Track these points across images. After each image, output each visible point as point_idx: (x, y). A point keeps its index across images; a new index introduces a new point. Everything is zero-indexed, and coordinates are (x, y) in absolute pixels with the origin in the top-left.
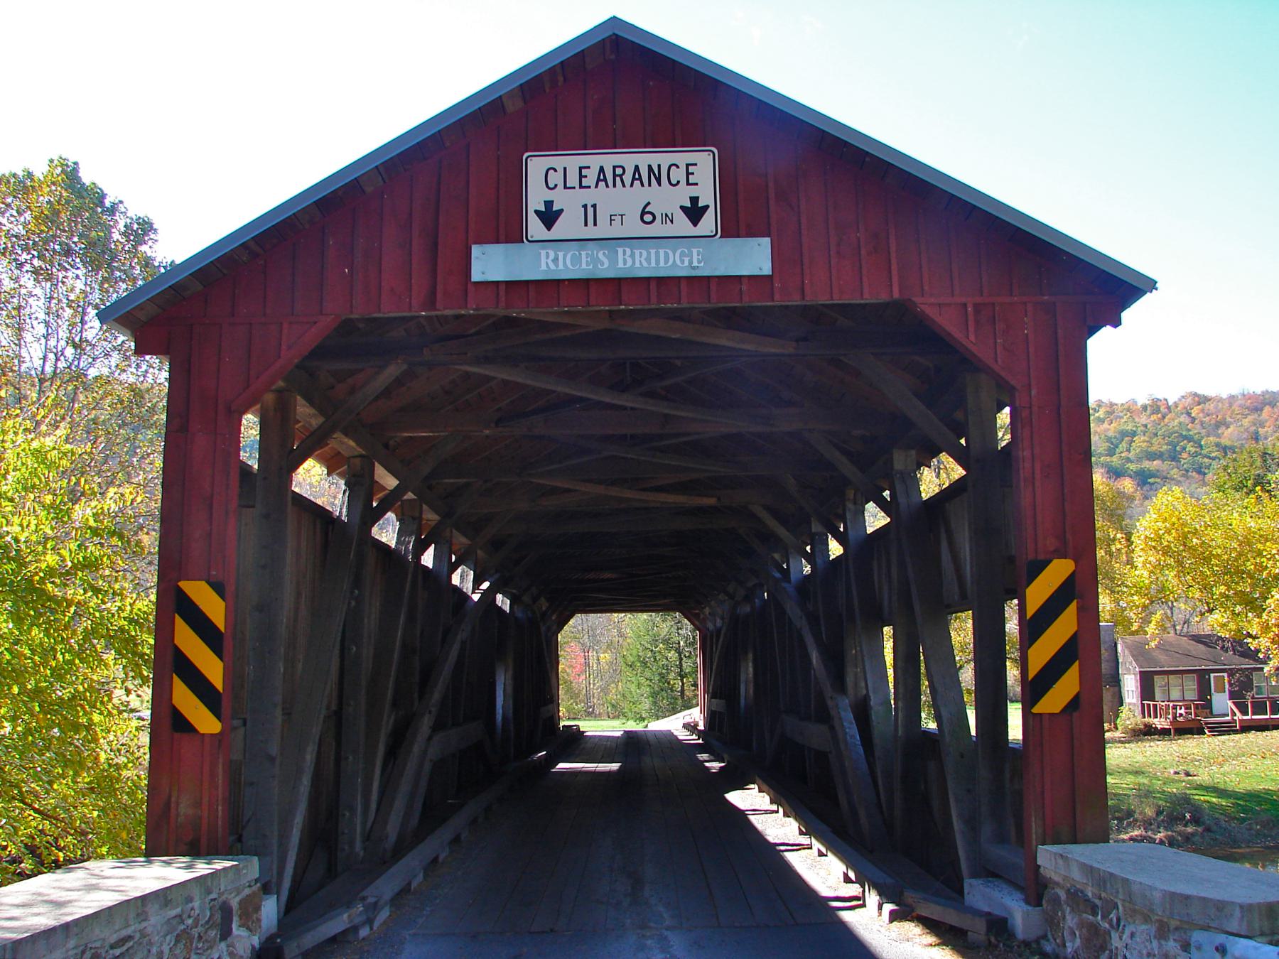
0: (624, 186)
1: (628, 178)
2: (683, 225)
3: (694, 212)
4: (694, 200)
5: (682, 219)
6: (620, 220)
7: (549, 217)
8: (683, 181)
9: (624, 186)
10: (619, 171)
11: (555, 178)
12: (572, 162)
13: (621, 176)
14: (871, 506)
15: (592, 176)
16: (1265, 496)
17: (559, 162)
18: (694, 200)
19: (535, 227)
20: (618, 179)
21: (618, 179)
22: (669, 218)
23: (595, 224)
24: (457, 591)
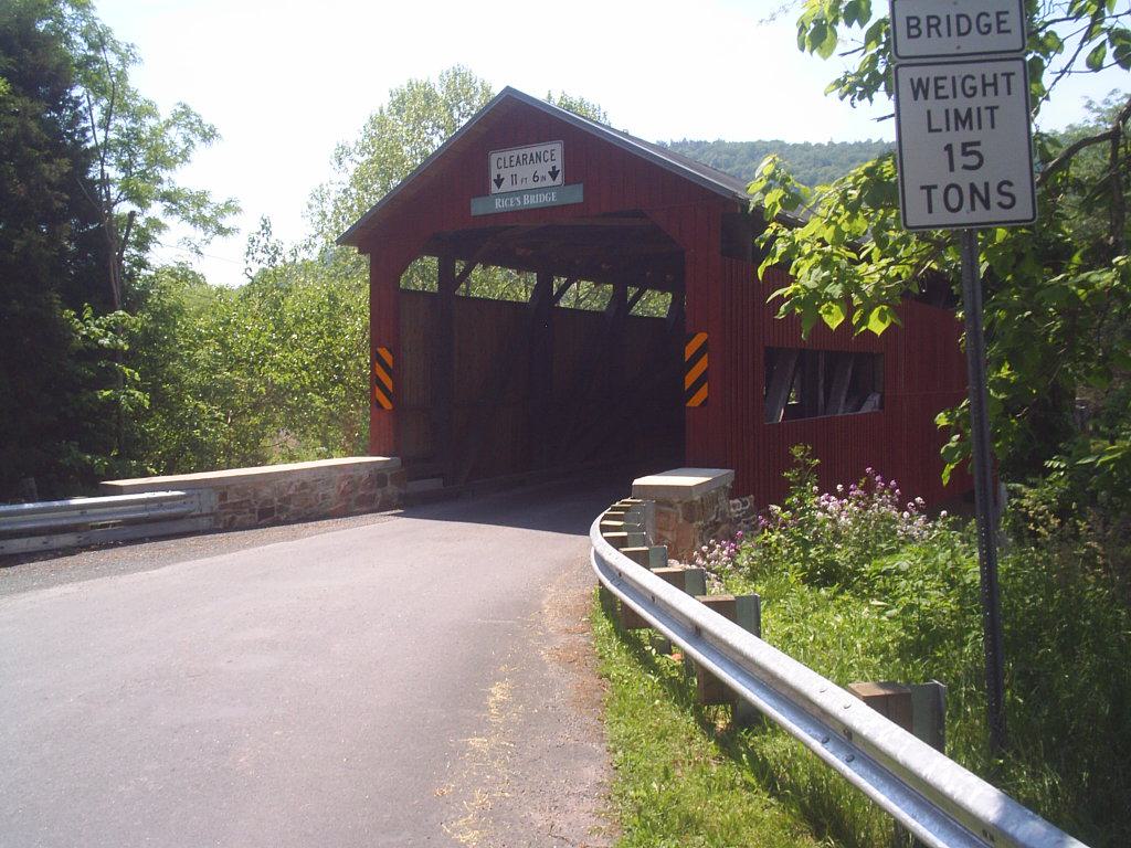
0: (940, 35)
1: (943, 28)
2: (549, 182)
3: (554, 174)
4: (554, 168)
5: (549, 177)
6: (527, 180)
7: (499, 182)
8: (994, 27)
9: (940, 35)
10: (933, 22)
11: (501, 163)
12: (507, 154)
13: (936, 26)
14: (432, 262)
15: (515, 159)
16: (324, 186)
17: (502, 155)
18: (554, 168)
19: (494, 188)
20: (933, 30)
21: (933, 30)
22: (544, 178)
23: (947, 111)
24: (748, 495)
